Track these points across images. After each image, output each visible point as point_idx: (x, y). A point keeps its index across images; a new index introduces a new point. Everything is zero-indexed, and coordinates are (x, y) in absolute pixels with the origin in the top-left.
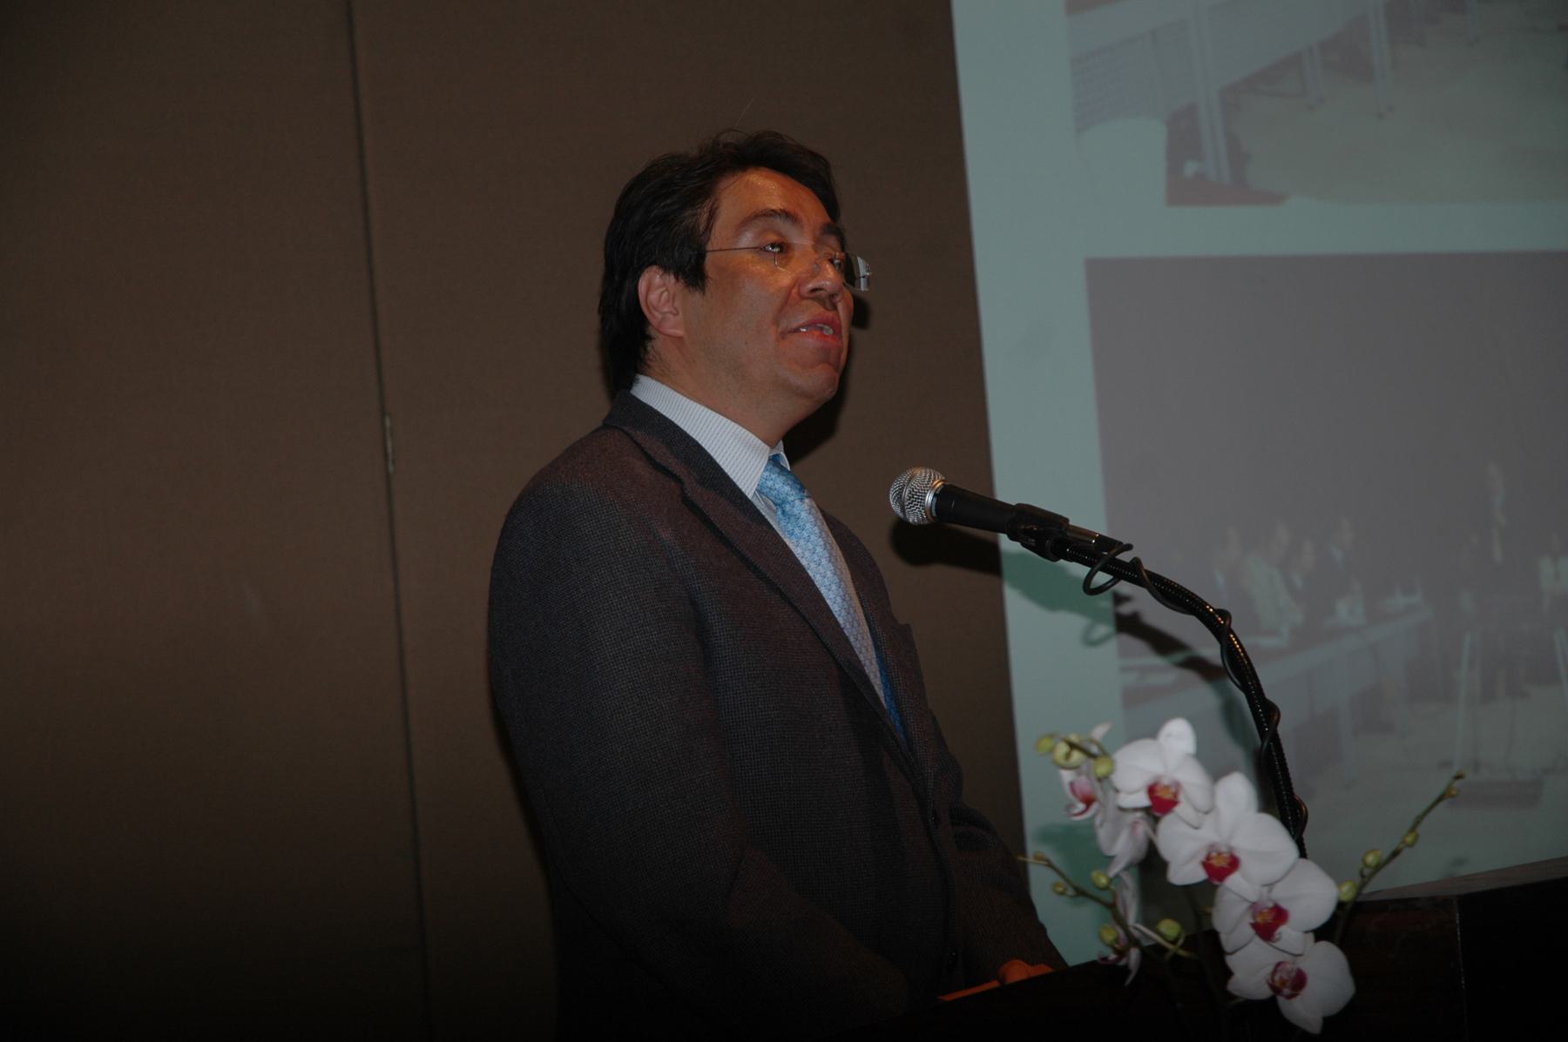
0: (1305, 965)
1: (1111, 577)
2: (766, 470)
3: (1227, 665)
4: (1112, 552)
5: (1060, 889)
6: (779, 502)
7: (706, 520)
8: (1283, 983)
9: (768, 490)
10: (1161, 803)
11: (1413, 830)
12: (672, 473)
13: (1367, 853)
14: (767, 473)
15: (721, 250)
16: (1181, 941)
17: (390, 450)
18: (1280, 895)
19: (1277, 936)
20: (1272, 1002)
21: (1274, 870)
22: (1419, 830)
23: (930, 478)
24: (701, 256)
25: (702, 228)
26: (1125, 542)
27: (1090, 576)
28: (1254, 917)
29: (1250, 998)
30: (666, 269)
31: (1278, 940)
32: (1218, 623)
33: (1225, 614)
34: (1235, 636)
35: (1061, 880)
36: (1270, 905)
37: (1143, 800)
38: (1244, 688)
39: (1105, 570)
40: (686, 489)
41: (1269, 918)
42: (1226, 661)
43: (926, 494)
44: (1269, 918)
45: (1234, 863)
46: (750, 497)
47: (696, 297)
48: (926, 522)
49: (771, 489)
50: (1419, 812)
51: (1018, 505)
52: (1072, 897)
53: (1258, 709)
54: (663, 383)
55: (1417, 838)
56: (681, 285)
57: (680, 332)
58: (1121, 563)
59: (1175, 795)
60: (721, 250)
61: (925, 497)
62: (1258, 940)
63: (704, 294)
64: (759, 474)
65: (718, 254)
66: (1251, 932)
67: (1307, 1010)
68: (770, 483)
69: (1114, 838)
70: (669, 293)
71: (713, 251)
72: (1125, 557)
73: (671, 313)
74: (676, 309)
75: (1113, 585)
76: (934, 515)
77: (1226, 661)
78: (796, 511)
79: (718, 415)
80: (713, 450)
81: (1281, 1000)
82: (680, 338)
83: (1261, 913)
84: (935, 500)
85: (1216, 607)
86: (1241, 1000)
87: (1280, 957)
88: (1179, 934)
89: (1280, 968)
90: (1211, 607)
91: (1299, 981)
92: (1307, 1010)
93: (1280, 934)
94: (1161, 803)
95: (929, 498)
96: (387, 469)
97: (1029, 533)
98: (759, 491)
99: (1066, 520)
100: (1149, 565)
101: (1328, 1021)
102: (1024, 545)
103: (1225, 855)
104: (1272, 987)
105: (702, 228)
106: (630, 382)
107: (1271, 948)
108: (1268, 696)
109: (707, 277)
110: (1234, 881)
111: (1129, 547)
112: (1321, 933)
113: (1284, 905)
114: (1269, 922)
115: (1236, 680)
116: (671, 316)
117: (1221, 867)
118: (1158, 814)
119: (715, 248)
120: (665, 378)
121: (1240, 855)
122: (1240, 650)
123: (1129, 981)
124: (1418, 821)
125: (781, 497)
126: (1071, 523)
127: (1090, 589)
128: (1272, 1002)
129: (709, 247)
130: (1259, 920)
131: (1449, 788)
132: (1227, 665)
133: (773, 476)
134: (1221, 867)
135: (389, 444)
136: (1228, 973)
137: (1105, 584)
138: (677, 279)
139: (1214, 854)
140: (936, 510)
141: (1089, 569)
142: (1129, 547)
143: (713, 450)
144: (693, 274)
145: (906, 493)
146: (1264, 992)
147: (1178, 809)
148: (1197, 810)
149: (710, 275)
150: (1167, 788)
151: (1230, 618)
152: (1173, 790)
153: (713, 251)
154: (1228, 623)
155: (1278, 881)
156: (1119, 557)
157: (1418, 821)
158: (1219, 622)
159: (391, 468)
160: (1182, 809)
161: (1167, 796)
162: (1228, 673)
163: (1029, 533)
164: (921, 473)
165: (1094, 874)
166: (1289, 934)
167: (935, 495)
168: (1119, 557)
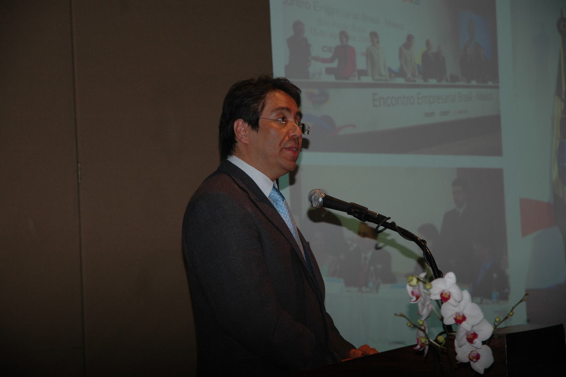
0: (480, 352)
1: (384, 227)
2: (272, 190)
3: (425, 257)
4: (385, 220)
5: (409, 325)
6: (275, 200)
7: (257, 207)
8: (473, 357)
9: (272, 196)
10: (444, 298)
11: (512, 311)
12: (245, 190)
13: (496, 318)
14: (272, 191)
15: (265, 118)
16: (443, 344)
17: (79, 175)
18: (475, 329)
19: (474, 342)
20: (469, 363)
21: (477, 321)
22: (514, 310)
23: (321, 193)
24: (258, 120)
25: (259, 110)
26: (387, 216)
27: (378, 227)
28: (467, 336)
29: (462, 361)
30: (245, 121)
31: (475, 343)
32: (421, 244)
33: (424, 241)
34: (428, 248)
35: (409, 322)
36: (462, 314)
37: (438, 297)
38: (431, 266)
39: (382, 225)
40: (250, 196)
41: (471, 337)
42: (425, 256)
43: (319, 198)
44: (471, 337)
45: (464, 318)
46: (267, 197)
47: (254, 133)
48: (319, 207)
49: (273, 196)
50: (514, 305)
51: (351, 203)
52: (412, 327)
53: (436, 272)
54: (240, 158)
55: (513, 313)
56: (250, 127)
57: (247, 142)
58: (388, 223)
59: (449, 296)
60: (265, 118)
61: (319, 199)
62: (468, 343)
63: (257, 132)
64: (270, 191)
65: (263, 119)
66: (466, 340)
67: (479, 367)
68: (273, 194)
69: (423, 310)
70: (244, 129)
71: (262, 118)
72: (389, 221)
73: (245, 135)
74: (247, 135)
75: (384, 230)
76: (322, 205)
77: (425, 256)
78: (281, 204)
79: (258, 171)
80: (259, 185)
81: (472, 363)
82: (247, 144)
83: (459, 315)
84: (323, 200)
85: (421, 239)
86: (459, 362)
87: (474, 349)
88: (443, 342)
89: (472, 353)
90: (419, 239)
91: (478, 357)
92: (479, 367)
93: (475, 341)
94: (444, 298)
95: (321, 200)
96: (78, 182)
97: (356, 212)
98: (269, 197)
99: (367, 209)
100: (398, 224)
101: (486, 370)
102: (354, 216)
103: (461, 316)
104: (469, 358)
105: (259, 110)
106: (227, 158)
107: (471, 346)
108: (439, 269)
109: (259, 127)
110: (464, 324)
111: (389, 218)
112: (484, 343)
113: (477, 333)
114: (472, 337)
115: (428, 263)
116: (244, 136)
117: (460, 319)
118: (443, 302)
119: (263, 117)
120: (241, 157)
121: (466, 316)
122: (429, 253)
123: (425, 355)
124: (513, 308)
125: (276, 199)
126: (369, 210)
127: (379, 231)
128: (469, 364)
129: (261, 117)
130: (469, 337)
131: (523, 298)
132: (425, 257)
133: (274, 192)
134: (460, 319)
135: (79, 173)
136: (456, 354)
137: (382, 230)
138: (249, 125)
139: (458, 316)
140: (323, 203)
141: (377, 225)
142: (389, 218)
143: (259, 185)
144: (254, 124)
145: (313, 198)
146: (466, 360)
147: (449, 301)
148: (456, 301)
149: (261, 127)
150: (446, 294)
151: (426, 242)
152: (448, 294)
153: (262, 118)
154: (425, 244)
155: (475, 326)
156: (387, 221)
157: (513, 308)
158: (422, 244)
159: (80, 181)
160: (451, 301)
161: (447, 296)
162: (425, 260)
163: (356, 212)
164: (318, 191)
165: (418, 320)
166: (478, 342)
167: (323, 198)
168: (387, 221)
